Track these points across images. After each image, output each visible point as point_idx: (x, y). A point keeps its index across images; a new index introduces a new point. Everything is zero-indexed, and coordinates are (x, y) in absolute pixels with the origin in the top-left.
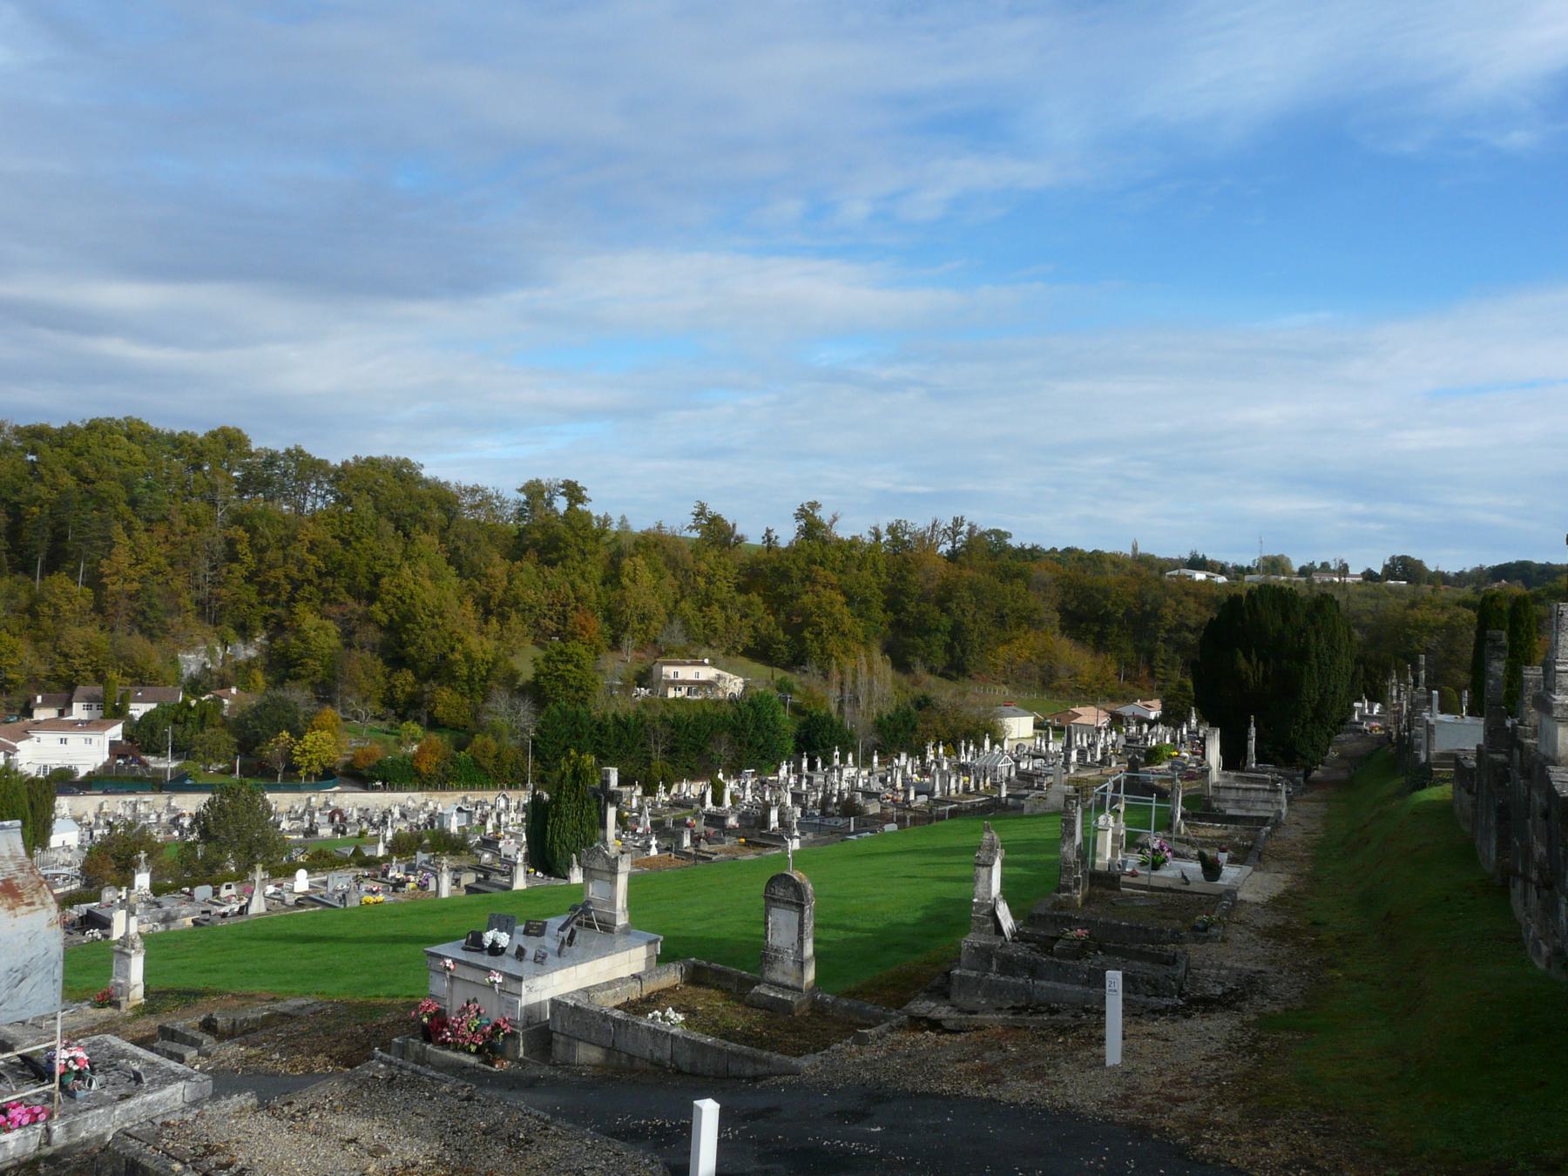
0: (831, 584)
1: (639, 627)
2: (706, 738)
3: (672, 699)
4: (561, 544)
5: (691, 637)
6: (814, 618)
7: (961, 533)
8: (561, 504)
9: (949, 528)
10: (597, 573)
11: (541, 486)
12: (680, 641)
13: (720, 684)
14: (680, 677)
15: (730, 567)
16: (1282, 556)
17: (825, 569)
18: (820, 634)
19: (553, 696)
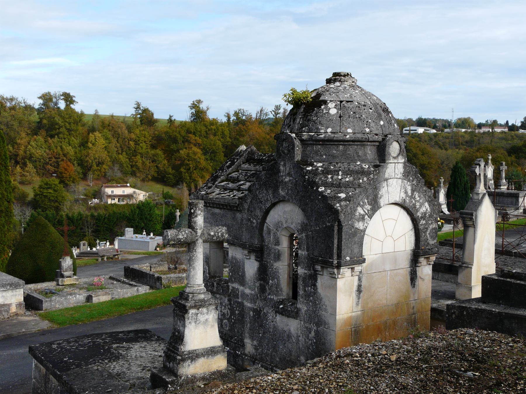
0: (198, 144)
1: (97, 168)
2: (114, 224)
3: (110, 204)
4: (57, 127)
5: (125, 173)
6: (186, 162)
7: (279, 113)
8: (62, 105)
9: (273, 111)
10: (76, 141)
11: (51, 95)
12: (119, 174)
13: (135, 196)
14: (115, 193)
15: (147, 135)
16: (469, 118)
17: (196, 136)
18: (189, 169)
19: (42, 205)
